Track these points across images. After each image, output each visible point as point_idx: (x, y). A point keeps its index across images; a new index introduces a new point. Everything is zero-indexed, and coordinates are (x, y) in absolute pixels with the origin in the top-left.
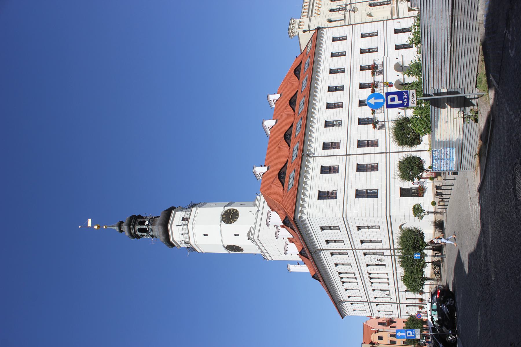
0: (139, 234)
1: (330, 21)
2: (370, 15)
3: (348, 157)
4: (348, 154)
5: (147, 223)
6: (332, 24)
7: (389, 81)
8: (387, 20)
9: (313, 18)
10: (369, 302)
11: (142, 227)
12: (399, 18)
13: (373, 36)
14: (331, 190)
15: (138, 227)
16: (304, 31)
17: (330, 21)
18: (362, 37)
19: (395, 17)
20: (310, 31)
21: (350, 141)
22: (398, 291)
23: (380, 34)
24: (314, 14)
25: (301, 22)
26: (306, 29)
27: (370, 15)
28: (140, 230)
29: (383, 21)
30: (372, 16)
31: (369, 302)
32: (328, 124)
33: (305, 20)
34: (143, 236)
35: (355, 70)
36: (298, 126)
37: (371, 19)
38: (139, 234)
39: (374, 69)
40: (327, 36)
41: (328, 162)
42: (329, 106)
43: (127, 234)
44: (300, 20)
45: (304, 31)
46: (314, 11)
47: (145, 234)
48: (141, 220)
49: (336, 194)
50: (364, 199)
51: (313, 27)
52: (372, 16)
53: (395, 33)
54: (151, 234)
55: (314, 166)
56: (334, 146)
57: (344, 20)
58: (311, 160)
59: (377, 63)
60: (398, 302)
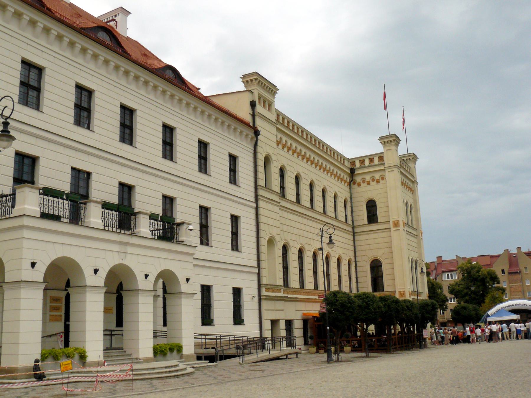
6: (261, 163)
8: (259, 274)
9: (274, 130)
16: (253, 105)
19: (264, 293)
24: (279, 135)
27: (271, 242)
37: (264, 242)
53: (203, 286)
56: (168, 148)
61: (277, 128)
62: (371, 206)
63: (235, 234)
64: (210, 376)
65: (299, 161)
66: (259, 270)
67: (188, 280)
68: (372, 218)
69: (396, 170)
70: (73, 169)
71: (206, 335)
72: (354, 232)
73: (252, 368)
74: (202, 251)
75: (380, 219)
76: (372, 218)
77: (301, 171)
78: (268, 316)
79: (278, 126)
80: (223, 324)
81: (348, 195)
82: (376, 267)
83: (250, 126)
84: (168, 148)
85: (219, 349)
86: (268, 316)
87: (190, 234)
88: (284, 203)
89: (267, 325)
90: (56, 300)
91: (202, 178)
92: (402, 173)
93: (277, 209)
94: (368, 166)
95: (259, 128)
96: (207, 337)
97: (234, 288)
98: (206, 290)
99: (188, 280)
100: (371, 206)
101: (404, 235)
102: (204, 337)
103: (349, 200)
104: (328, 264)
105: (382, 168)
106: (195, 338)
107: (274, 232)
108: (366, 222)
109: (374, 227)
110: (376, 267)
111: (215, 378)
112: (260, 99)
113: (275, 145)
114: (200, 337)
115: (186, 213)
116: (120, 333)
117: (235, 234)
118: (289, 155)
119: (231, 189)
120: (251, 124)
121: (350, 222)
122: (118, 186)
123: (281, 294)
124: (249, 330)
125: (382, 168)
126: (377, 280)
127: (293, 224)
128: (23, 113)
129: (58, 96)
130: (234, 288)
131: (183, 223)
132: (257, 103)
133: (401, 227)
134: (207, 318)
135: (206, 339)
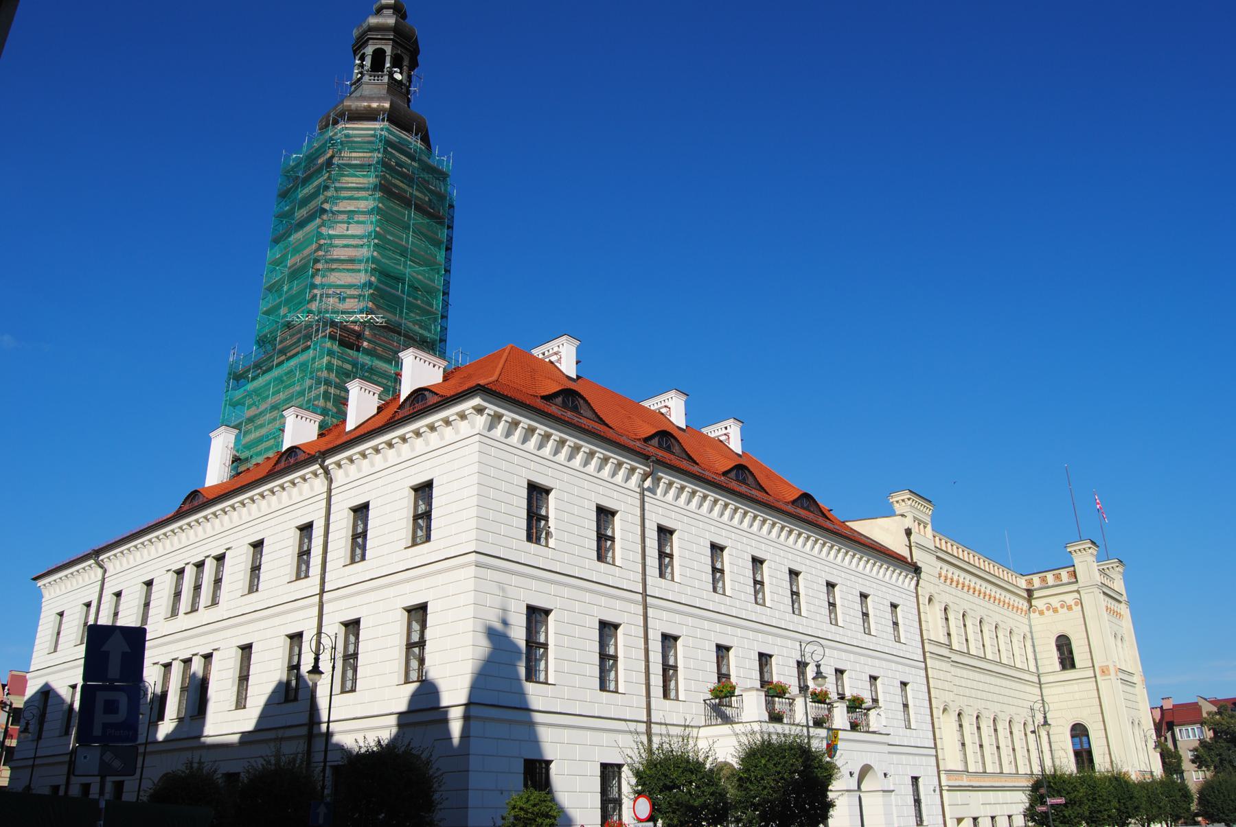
0: (369, 50)
5: (398, 76)
8: (937, 756)
10: (35, 758)
11: (388, 59)
12: (941, 791)
15: (388, 50)
16: (908, 532)
18: (761, 655)
22: (276, 739)
24: (940, 564)
26: (912, 538)
28: (379, 56)
31: (33, 766)
34: (362, 58)
36: (695, 469)
38: (369, 50)
40: (894, 583)
41: (622, 528)
43: (373, 20)
44: (929, 527)
45: (908, 532)
47: (368, 63)
48: (406, 63)
51: (919, 557)
53: (604, 766)
54: (366, 78)
60: (38, 761)
61: (938, 558)
62: (1064, 646)
63: (607, 660)
67: (885, 775)
68: (1067, 660)
69: (1097, 591)
72: (1040, 683)
76: (1067, 660)
82: (1079, 731)
83: (907, 562)
92: (1105, 593)
95: (919, 564)
97: (602, 765)
100: (1064, 646)
103: (1029, 635)
107: (948, 697)
108: (1058, 667)
109: (1070, 674)
110: (1079, 731)
117: (607, 660)
119: (866, 641)
121: (1033, 669)
125: (1074, 587)
126: (1084, 756)
127: (992, 689)
130: (602, 765)
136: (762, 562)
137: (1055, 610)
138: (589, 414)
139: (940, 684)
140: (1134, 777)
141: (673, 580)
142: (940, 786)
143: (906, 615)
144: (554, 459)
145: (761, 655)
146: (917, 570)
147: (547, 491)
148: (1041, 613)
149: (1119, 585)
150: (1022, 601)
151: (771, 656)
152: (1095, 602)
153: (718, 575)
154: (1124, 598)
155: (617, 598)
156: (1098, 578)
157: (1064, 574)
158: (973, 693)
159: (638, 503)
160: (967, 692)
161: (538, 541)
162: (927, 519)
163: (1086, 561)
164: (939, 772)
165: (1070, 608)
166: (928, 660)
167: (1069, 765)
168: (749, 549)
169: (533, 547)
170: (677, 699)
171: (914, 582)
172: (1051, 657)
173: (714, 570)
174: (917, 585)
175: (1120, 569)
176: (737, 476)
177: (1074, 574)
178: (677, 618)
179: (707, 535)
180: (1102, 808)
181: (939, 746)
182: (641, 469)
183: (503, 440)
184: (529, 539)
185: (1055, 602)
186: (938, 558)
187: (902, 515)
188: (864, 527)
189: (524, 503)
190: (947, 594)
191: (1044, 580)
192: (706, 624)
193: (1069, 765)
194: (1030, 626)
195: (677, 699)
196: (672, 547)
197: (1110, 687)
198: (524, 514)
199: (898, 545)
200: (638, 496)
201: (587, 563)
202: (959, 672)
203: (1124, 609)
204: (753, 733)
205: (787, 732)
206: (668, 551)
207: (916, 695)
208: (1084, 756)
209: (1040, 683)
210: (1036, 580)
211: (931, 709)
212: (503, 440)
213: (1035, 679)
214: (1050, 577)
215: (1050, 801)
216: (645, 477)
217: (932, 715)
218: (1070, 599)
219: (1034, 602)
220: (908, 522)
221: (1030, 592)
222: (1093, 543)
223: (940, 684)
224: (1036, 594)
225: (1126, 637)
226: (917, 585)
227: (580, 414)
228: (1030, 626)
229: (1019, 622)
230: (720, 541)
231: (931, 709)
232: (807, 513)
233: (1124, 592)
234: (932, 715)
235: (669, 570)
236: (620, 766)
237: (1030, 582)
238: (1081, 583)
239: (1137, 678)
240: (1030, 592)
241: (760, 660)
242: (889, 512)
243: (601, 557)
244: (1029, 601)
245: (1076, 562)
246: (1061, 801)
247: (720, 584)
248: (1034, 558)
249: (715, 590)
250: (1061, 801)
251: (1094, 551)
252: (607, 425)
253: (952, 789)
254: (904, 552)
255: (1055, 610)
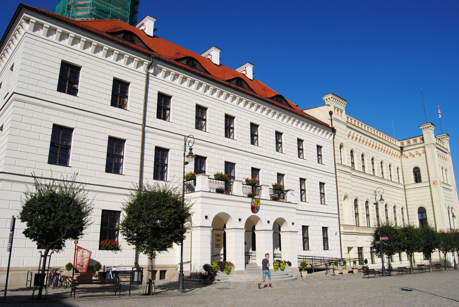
1: (341, 146)
2: (345, 197)
3: (141, 127)
4: (146, 128)
7: (261, 207)
8: (339, 218)
12: (340, 234)
13: (304, 243)
14: (80, 87)
16: (331, 113)
17: (341, 146)
18: (320, 183)
19: (342, 230)
20: (331, 120)
21: (168, 137)
23: (322, 208)
24: (349, 130)
25: (341, 112)
26: (333, 116)
27: (345, 197)
29: (339, 214)
30: (344, 199)
32: (201, 111)
33: (344, 117)
35: (278, 166)
37: (341, 198)
39: (279, 193)
40: (323, 138)
41: (134, 95)
42: (229, 119)
44: (344, 112)
45: (331, 113)
46: (353, 132)
49: (69, 93)
50: (49, 139)
51: (335, 125)
52: (344, 199)
53: (323, 228)
55: (133, 71)
56: (229, 130)
57: (374, 175)
58: (142, 69)
59: (288, 194)
61: (348, 127)
62: (417, 171)
64: (306, 281)
65: (389, 156)
66: (339, 216)
67: (293, 224)
68: (418, 179)
69: (433, 146)
70: (226, 162)
71: (315, 257)
72: (405, 189)
73: (333, 278)
74: (302, 206)
75: (423, 180)
76: (418, 179)
77: (364, 151)
78: (345, 245)
79: (348, 125)
80: (316, 250)
81: (399, 165)
82: (422, 211)
83: (330, 127)
84: (229, 130)
85: (314, 265)
86: (345, 245)
87: (292, 196)
88: (354, 173)
89: (345, 250)
90: (218, 235)
91: (319, 166)
92: (437, 148)
93: (349, 177)
94: (412, 145)
96: (306, 257)
98: (305, 228)
99: (293, 224)
100: (417, 171)
101: (442, 190)
102: (304, 257)
104: (367, 207)
105: (422, 145)
106: (299, 258)
107: (348, 191)
108: (413, 181)
109: (419, 185)
110: (422, 211)
111: (309, 283)
112: (335, 109)
113: (347, 137)
114: (302, 257)
115: (291, 183)
116: (254, 254)
118: (367, 147)
120: (330, 126)
121: (401, 182)
122: (107, 139)
123: (355, 231)
124: (333, 253)
125: (422, 145)
126: (423, 221)
128: (198, 133)
129: (215, 121)
131: (289, 190)
132: (333, 112)
133: (439, 185)
134: (306, 246)
135: (305, 259)
136: (321, 147)
137: (413, 156)
138: (141, 44)
139: (343, 185)
140: (446, 232)
141: (258, 146)
142: (340, 232)
143: (327, 152)
144: (267, 116)
145: (320, 183)
146: (333, 131)
147: (233, 118)
148: (407, 157)
149: (447, 145)
150: (397, 152)
151: (205, 158)
152: (432, 152)
153: (320, 157)
154: (449, 151)
155: (278, 163)
156: (434, 140)
157: (418, 140)
158: (365, 191)
159: (144, 79)
160: (361, 190)
161: (164, 119)
162: (343, 109)
163: (429, 133)
164: (340, 225)
165: (420, 155)
166: (337, 173)
167: (416, 224)
168: (249, 119)
169: (227, 139)
170: (306, 202)
171: (332, 137)
172: (411, 177)
173: (318, 155)
174: (334, 138)
175: (448, 138)
176: (187, 62)
177: (423, 139)
178: (324, 177)
179: (315, 142)
180: (415, 243)
181: (340, 213)
182: (147, 62)
183: (188, 88)
184: (226, 136)
185: (413, 152)
186: (348, 127)
187: (328, 105)
188: (311, 112)
189: (224, 122)
190: (350, 144)
191: (409, 142)
192: (316, 174)
193: (416, 224)
194: (402, 163)
195: (306, 202)
196: (281, 140)
197: (438, 191)
198: (224, 127)
199: (325, 119)
200: (145, 76)
201: (272, 152)
202: (353, 179)
203: (449, 157)
204: (66, 188)
205: (48, 184)
206: (280, 141)
207: (329, 190)
208: (423, 221)
209: (405, 189)
210: (405, 143)
211: (337, 196)
212: (188, 88)
213: (403, 187)
214: (412, 141)
215: (381, 238)
216: (149, 67)
217: (338, 199)
218: (420, 151)
219: (403, 153)
220: (331, 109)
221: (402, 148)
222: (432, 124)
223: (343, 185)
224: (405, 149)
225: (448, 169)
226: (334, 138)
227: (136, 44)
228: (402, 163)
229: (396, 162)
230: (320, 144)
231: (337, 196)
232: (278, 102)
233: (449, 149)
234: (338, 199)
235: (302, 155)
236: (120, 212)
237: (402, 144)
238: (425, 143)
239: (453, 187)
240: (402, 148)
241: (278, 176)
242: (323, 104)
243: (253, 143)
244: (401, 152)
245: (424, 133)
246: (386, 238)
247: (320, 160)
248: (404, 131)
249: (318, 162)
250: (386, 238)
251: (433, 128)
252: (152, 51)
253: (346, 233)
254: (329, 123)
255: (413, 156)
